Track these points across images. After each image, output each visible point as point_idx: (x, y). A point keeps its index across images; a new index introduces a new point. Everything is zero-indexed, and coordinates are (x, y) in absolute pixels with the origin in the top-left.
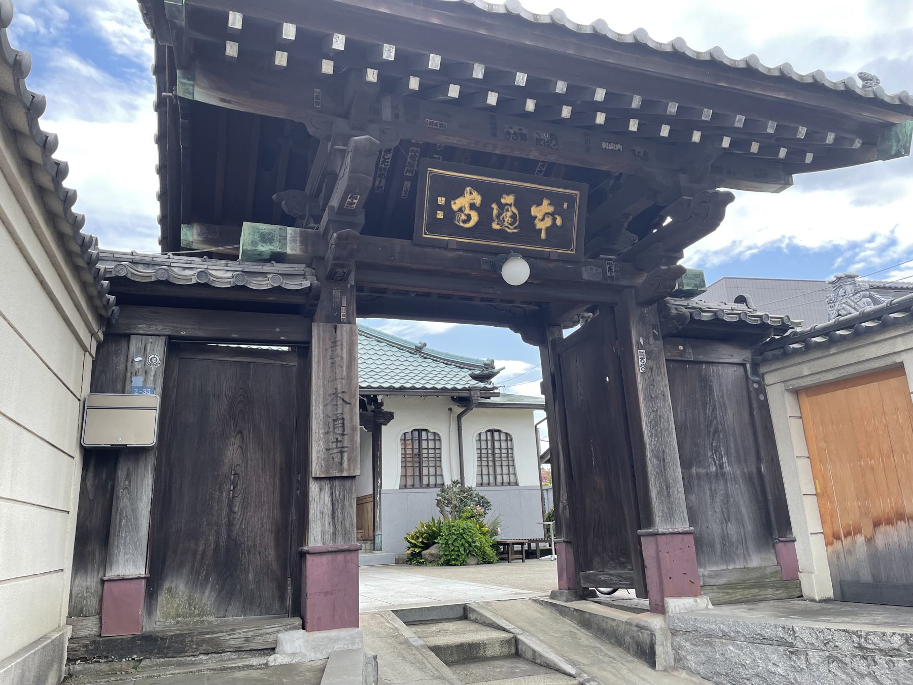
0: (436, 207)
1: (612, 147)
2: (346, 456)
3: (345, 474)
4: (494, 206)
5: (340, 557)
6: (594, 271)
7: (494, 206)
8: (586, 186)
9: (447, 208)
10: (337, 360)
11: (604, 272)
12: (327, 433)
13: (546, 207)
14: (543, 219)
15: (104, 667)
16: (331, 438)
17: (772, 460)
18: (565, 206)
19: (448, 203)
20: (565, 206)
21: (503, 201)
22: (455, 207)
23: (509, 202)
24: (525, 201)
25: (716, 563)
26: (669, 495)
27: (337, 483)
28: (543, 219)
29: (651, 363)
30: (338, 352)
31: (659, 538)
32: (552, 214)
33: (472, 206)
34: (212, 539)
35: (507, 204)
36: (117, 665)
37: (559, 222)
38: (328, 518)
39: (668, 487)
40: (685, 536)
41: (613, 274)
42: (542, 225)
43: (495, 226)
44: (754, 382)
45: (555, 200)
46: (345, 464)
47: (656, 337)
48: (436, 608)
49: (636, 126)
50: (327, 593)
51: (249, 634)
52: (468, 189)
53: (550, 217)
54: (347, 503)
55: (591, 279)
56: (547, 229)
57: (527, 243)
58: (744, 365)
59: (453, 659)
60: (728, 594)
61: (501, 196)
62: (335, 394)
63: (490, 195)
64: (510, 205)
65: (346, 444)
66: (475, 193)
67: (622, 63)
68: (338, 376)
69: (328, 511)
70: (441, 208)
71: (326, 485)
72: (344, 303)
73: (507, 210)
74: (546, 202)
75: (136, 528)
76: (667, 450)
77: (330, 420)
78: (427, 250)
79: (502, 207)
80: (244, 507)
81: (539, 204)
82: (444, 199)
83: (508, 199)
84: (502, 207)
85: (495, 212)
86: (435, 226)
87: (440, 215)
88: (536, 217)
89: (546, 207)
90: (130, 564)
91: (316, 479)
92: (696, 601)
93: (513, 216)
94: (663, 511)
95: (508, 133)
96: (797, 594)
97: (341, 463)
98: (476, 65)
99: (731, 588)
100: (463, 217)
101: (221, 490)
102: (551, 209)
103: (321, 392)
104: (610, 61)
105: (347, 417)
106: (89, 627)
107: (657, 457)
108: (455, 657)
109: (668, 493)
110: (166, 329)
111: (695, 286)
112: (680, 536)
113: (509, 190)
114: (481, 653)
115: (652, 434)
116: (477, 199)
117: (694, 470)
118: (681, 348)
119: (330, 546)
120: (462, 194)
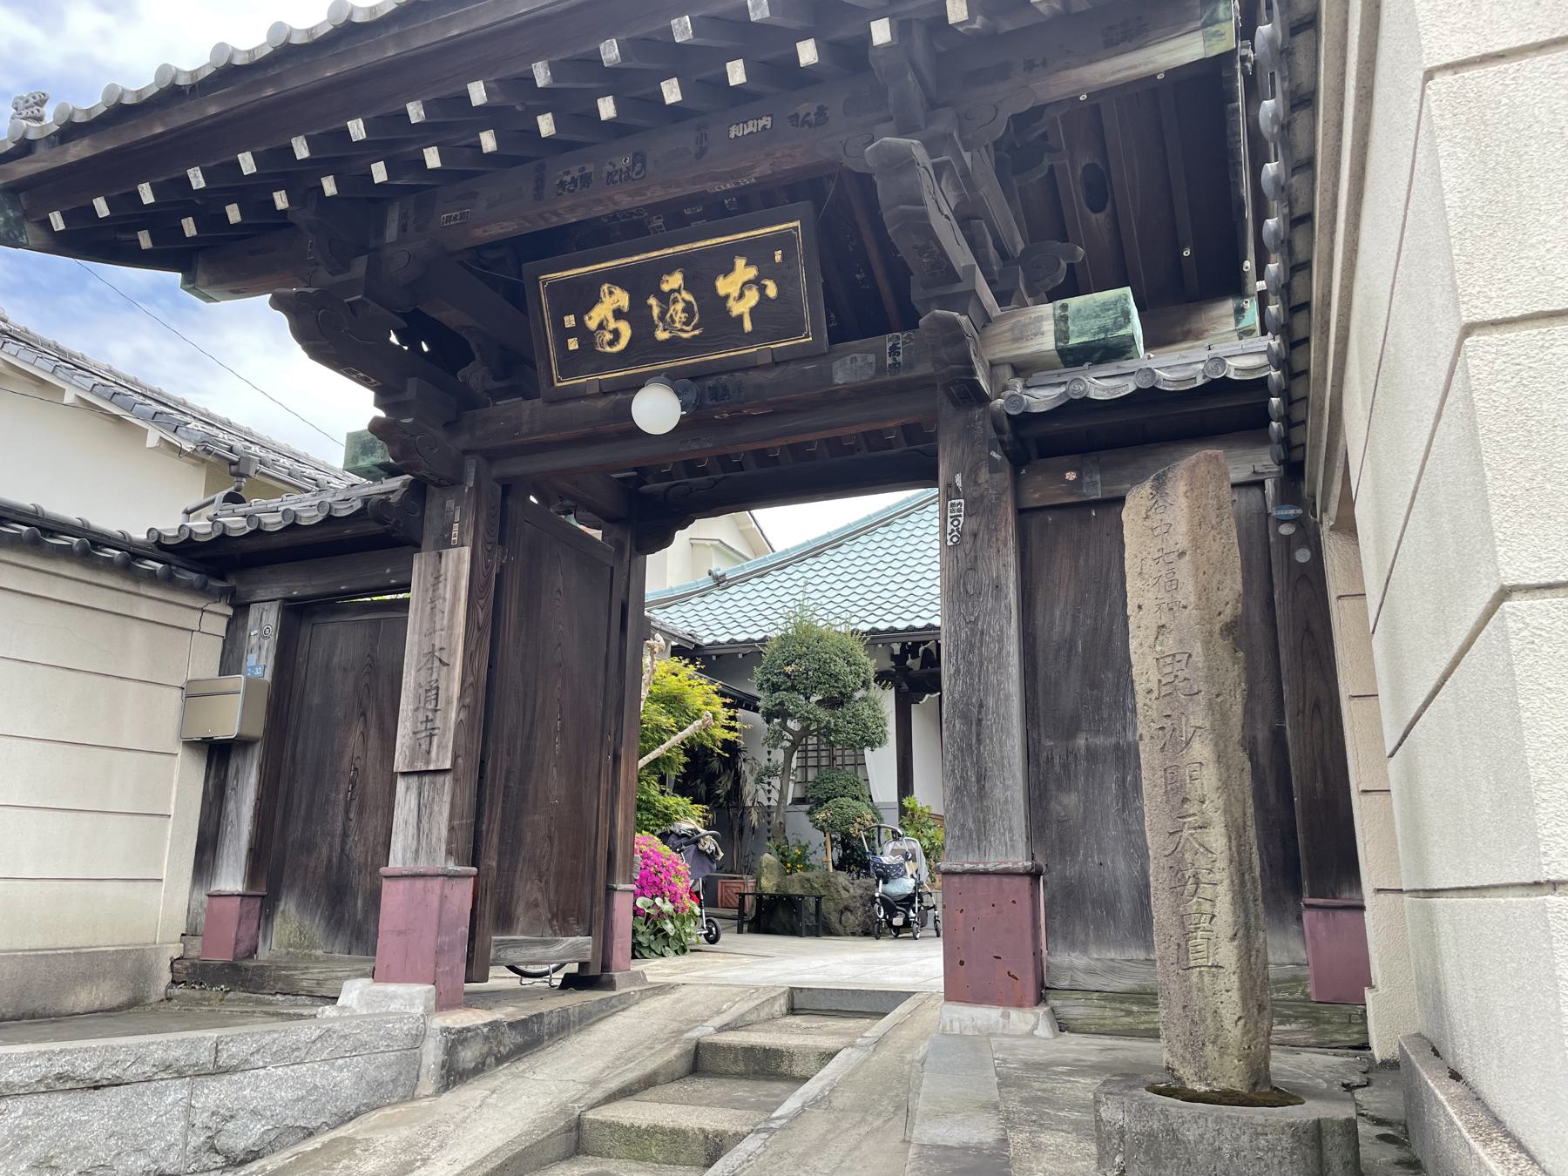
0: (563, 334)
1: (750, 128)
2: (435, 739)
3: (431, 768)
4: (652, 301)
5: (419, 883)
6: (859, 363)
7: (652, 301)
8: (805, 206)
9: (581, 330)
10: (439, 603)
11: (880, 360)
12: (417, 709)
13: (744, 271)
14: (741, 296)
15: (197, 994)
16: (422, 717)
17: (1317, 706)
18: (778, 257)
19: (580, 322)
20: (778, 257)
21: (666, 287)
22: (592, 324)
23: (676, 286)
24: (702, 274)
25: (1120, 944)
26: (982, 794)
27: (427, 779)
28: (741, 296)
29: (973, 524)
30: (441, 591)
31: (1438, 901)
32: (756, 282)
33: (618, 314)
34: (325, 851)
35: (673, 291)
36: (207, 994)
37: (772, 291)
38: (412, 830)
39: (981, 778)
40: (1006, 880)
41: (900, 358)
42: (741, 308)
43: (662, 335)
44: (1281, 521)
45: (756, 252)
46: (433, 754)
47: (994, 467)
48: (867, 992)
49: (677, 90)
50: (400, 933)
51: (321, 976)
52: (605, 287)
53: (755, 288)
54: (436, 808)
55: (853, 380)
56: (752, 311)
57: (727, 347)
58: (1260, 484)
59: (738, 1070)
60: (1129, 1013)
61: (659, 281)
62: (432, 653)
63: (641, 283)
64: (678, 291)
65: (438, 723)
66: (617, 291)
67: (475, 25)
68: (438, 627)
69: (413, 820)
70: (571, 333)
71: (414, 781)
72: (457, 518)
73: (675, 301)
74: (740, 263)
75: (238, 837)
76: (991, 702)
77: (422, 691)
78: (570, 405)
79: (665, 299)
80: (360, 813)
81: (728, 270)
82: (572, 317)
83: (674, 281)
84: (665, 299)
85: (656, 311)
86: (571, 365)
87: (573, 344)
88: (727, 297)
89: (744, 271)
90: (231, 878)
91: (404, 774)
92: (1006, 1016)
93: (688, 308)
94: (963, 826)
95: (562, 184)
96: (1355, 1038)
97: (429, 752)
98: (240, 156)
99: (1139, 1002)
100: (609, 336)
101: (337, 791)
102: (752, 272)
103: (415, 652)
104: (455, 33)
105: (442, 685)
106: (196, 949)
107: (965, 717)
108: (741, 1067)
109: (982, 788)
110: (278, 591)
111: (1104, 329)
112: (995, 879)
113: (668, 266)
114: (784, 1068)
115: (957, 671)
116: (622, 299)
117: (1081, 741)
118: (1071, 476)
119: (410, 867)
120: (597, 300)
